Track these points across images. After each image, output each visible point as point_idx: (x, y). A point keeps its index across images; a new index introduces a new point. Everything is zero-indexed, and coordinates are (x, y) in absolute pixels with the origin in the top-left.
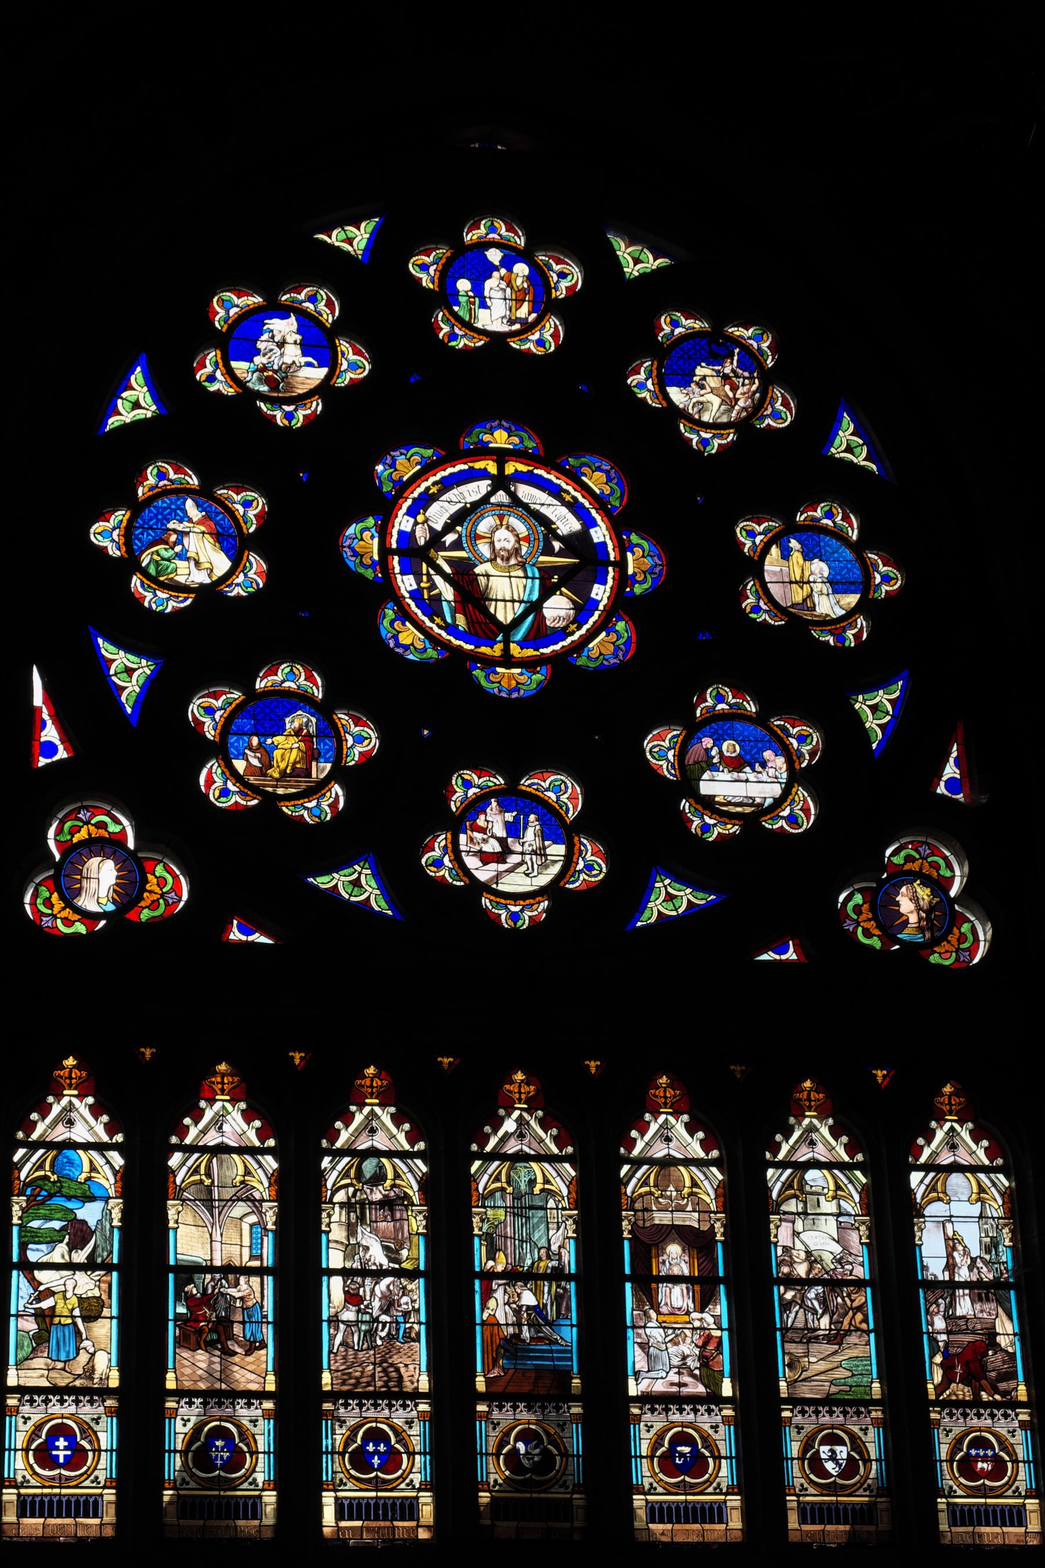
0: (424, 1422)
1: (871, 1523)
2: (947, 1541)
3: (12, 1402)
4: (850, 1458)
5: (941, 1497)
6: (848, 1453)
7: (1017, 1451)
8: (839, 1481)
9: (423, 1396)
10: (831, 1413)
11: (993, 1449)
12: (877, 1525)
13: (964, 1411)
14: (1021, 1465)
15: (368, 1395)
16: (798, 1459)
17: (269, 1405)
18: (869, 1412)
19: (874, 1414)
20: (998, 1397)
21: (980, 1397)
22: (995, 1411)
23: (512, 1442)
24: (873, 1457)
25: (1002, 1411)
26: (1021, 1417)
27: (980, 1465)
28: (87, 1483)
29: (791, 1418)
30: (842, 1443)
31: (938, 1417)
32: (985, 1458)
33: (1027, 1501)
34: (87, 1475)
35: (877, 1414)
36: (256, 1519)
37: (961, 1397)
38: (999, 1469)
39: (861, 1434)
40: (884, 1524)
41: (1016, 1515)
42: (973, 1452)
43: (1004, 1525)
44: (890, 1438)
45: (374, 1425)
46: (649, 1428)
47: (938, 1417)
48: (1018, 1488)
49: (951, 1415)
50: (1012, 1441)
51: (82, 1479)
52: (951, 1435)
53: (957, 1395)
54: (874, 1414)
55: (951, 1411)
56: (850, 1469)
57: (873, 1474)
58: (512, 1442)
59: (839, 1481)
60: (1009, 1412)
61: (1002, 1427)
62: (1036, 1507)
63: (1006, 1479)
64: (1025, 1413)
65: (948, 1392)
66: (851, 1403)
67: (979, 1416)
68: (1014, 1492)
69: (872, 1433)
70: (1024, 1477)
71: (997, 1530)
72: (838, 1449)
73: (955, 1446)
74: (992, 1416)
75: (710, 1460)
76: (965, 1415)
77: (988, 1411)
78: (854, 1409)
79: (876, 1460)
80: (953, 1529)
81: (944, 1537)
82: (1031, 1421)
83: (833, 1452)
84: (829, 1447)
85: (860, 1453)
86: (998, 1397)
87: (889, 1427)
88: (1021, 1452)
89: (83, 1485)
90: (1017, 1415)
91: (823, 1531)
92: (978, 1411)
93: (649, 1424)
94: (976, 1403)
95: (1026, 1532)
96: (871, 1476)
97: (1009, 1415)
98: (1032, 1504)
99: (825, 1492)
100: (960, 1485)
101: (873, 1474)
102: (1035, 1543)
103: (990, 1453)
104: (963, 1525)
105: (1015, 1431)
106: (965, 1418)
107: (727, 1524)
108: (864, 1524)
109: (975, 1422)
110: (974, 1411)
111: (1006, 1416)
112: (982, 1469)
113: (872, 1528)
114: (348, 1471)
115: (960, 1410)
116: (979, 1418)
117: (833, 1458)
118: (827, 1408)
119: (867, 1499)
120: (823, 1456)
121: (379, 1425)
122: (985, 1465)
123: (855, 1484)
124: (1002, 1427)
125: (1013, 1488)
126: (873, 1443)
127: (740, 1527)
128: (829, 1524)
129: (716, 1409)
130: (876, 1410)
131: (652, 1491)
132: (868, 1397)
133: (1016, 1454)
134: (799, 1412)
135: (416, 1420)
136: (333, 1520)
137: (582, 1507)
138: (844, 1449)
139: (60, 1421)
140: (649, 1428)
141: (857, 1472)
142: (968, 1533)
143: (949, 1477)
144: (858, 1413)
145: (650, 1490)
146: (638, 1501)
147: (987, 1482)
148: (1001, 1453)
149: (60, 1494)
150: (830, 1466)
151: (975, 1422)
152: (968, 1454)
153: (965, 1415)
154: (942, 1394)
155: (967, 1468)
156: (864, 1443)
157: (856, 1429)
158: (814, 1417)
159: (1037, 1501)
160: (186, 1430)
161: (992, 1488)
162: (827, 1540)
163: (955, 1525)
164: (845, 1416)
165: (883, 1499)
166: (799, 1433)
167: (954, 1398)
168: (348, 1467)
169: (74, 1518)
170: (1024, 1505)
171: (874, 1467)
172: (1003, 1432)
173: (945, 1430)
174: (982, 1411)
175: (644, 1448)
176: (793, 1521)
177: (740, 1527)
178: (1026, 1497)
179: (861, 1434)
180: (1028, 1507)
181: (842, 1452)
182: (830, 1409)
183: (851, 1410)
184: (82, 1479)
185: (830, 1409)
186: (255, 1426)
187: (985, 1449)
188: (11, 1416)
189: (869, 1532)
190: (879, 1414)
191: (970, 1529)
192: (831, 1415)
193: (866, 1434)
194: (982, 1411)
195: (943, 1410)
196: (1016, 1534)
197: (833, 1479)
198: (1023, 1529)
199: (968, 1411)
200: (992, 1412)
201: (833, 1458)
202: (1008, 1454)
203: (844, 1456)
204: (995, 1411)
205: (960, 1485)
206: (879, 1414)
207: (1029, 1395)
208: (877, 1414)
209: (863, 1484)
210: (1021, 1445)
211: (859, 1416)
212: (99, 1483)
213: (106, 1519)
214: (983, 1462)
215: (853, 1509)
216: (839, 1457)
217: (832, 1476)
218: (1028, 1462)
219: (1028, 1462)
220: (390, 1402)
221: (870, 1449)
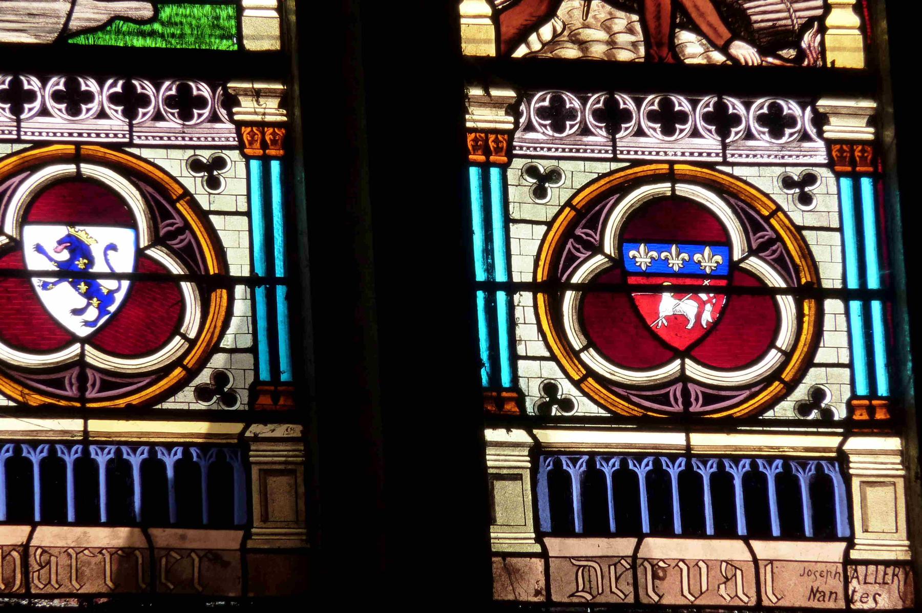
0: (266, 161)
1: (221, 522)
2: (527, 590)
3: (484, 115)
4: (146, 274)
5: (509, 423)
6: (140, 254)
7: (819, 253)
8: (96, 358)
9: (843, 83)
10: (74, 100)
11: (722, 241)
12: (247, 527)
13: (611, 103)
14: (833, 306)
15: (156, 64)
16: (533, 287)
17: (851, 121)
18: (230, 101)
19: (247, 109)
20: (745, 52)
21: (674, 49)
22: (735, 105)
23: (609, 246)
24: (239, 266)
25: (761, 105)
26: (837, 128)
27: (668, 305)
28: (185, 399)
29: (511, 133)
30: (114, 212)
31: (503, 120)
32: (687, 283)
33: (854, 443)
34: (782, 381)
35: (851, 121)
36: (831, 536)
37: (598, 51)
38: (745, 317)
39: (194, 183)
40: (276, 520)
41: (809, 502)
42: (642, 256)
43: (759, 529)
44: (302, 190)
45: (664, 188)
46: (542, 182)
47: (503, 120)
48: (818, 394)
49: (557, 116)
50: (799, 215)
51: (164, 384)
52: (558, 194)
53: (582, 44)
54: (247, 109)
55: (558, 102)
56: (147, 309)
57: (237, 333)
58: (609, 246)
59: (96, 358)
60: (791, 107)
61: (761, 163)
62: (893, 466)
63: (772, 359)
64: (854, 114)
65: (546, 32)
66: (156, 64)
67: (668, 120)
68: (803, 408)
69: (237, 176)
70: (844, 354)
71: (733, 550)
72: (96, 237)
73: (568, 233)
74: (722, 121)
75: (787, 305)
76: (613, 118)
77: (707, 103)
78: (169, 88)
79: (251, 282)
80: (555, 545)
81: (512, 573)
82: (877, 144)
83: (77, 248)
84: (61, 231)
85: (188, 255)
86: (745, 52)
87: (308, 158)
88: (832, 262)
89: (168, 405)
90: (820, 120)
91: (25, 549)
92: (666, 105)
93: (543, 166)
94: (660, 73)
95: (847, 561)
96: (227, 342)
97: (791, 121)
98: (876, 455)
99: (36, 400)
100: (587, 378)
101: (237, 333)
102: (884, 602)
103: (708, 260)
104: (595, 528)
105: (810, 179)
106: (613, 130)
107: (851, 542)
108: (197, 524)
109: (653, 143)
110: (652, 102)
111: (776, 123)
112: (678, 320)
113: (225, 540)
114: (573, 354)
115: (596, 100)
116: (668, 130)
117: (76, 270)
118: (57, 83)
119: (202, 427)
120: (34, 261)
121: (87, 169)
122: (688, 307)
123: (165, 371)
124: (761, 163)
125: (801, 393)
126: (239, 215)
127: (901, 553)
128: (48, 520)
129: (804, 118)
130: (257, 94)
131: (555, 411)
132: (225, 45)
133: (814, 267)
134: (542, 113)
135: (233, 156)
136: (232, 533)
137: (286, 471)
138: (123, 237)
139: (664, 188)
140: (542, 182)
141: (175, 327)
142: (614, 560)
143: (532, 352)
144: (185, 105)
145: (544, 408)
146: (505, 447)
147: (694, 370)
148: (756, 265)
149: (86, 439)
150: (62, 302)
151: (653, 143)
152: (618, 263)
153: (613, 118)
154: (522, 37)
155: (613, 314)
156: (203, 216)
157: (174, 164)
158: (600, 137)
159: (895, 443)
160: (544, 211)
161: (713, 394)
162: (37, 586)
163: (563, 529)
164: (130, 114)
165: (281, 431)
166: (540, 192)
167: (571, 52)
168: (576, 342)
169: (746, 540)
170: (842, 458)
171: (241, 307)
172: (766, 181)
173: (532, 171)
174: (681, 103)
175: (525, 253)
176: (513, 522)
177: (901, 553)
178: (850, 427)
179: (194, 183)
180: (857, 465)
181: (115, 249)
182: (72, 85)
183: (157, 93)
184: (164, 384)
185: (72, 85)
186: (213, 183)
187: (699, 243)
188: (485, 168)
189: (213, 556)
190: (270, 110)
191: (624, 546)
192: (74, 110)
193: (213, 183)
194: (681, 103)
195: (525, 94)
196: (807, 569)
197: (75, 349)
198: (833, 551)
199: (625, 101)
200: (721, 107)
201: (76, 270)
202: (781, 264)
203: (125, 262)
204: (735, 105)
205: (587, 378)
206: (270, 110)
207: (870, 48)
208: (263, 106)
209: (192, 373)
210: (836, 230)
211: (186, 115)
212: (230, 398)
213: (263, 535)
214: (679, 291)
215: (152, 466)
216: (99, 267)
217: (70, 339)
218: (864, 295)
219: (864, 295)
220: (184, 90)
221: (227, 240)
